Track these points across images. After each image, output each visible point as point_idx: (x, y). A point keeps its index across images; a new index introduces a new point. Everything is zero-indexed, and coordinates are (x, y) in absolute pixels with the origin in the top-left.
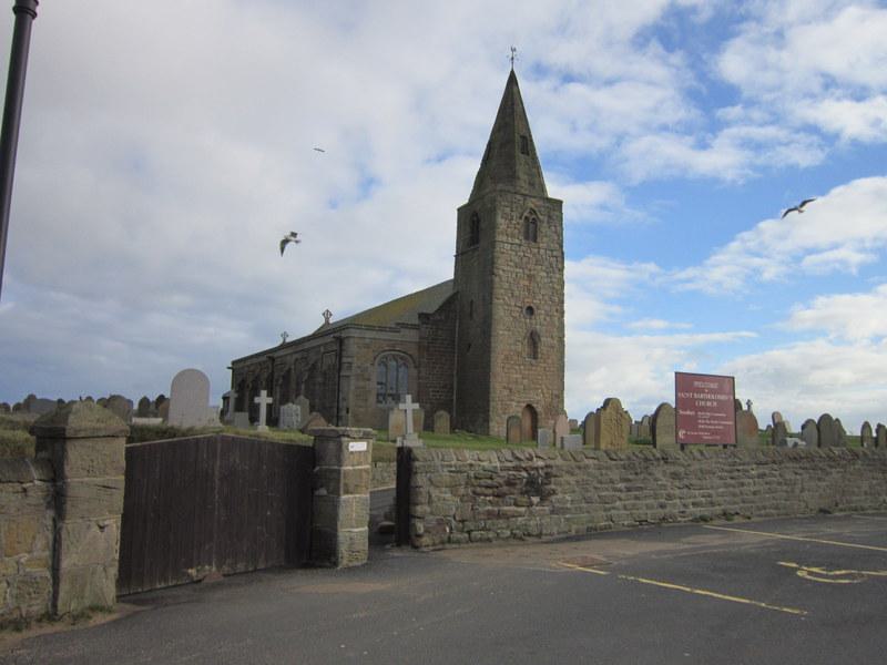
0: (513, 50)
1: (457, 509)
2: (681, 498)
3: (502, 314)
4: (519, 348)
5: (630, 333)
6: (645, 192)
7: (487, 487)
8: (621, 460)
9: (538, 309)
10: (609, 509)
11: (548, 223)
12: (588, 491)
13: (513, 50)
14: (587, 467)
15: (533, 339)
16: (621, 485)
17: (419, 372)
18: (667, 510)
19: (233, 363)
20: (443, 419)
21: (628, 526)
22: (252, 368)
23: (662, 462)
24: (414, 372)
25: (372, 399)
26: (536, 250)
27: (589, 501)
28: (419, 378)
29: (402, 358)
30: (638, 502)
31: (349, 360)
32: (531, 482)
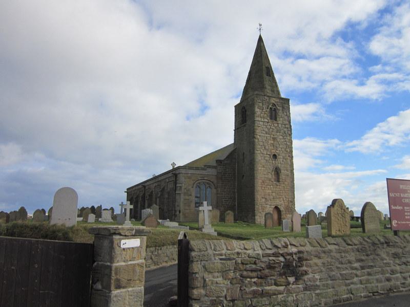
0: (260, 25)
1: (228, 290)
2: (401, 273)
3: (260, 159)
4: (270, 176)
5: (324, 172)
6: (332, 107)
7: (252, 271)
8: (355, 245)
9: (279, 155)
10: (349, 285)
11: (282, 110)
12: (333, 271)
13: (260, 25)
14: (330, 251)
15: (277, 171)
16: (357, 265)
17: (217, 191)
18: (392, 283)
19: (128, 189)
20: (230, 216)
21: (365, 297)
22: (136, 191)
23: (385, 245)
24: (214, 191)
25: (193, 205)
26: (277, 125)
27: (333, 278)
28: (217, 194)
29: (208, 183)
30: (370, 277)
31: (180, 185)
32: (288, 265)
